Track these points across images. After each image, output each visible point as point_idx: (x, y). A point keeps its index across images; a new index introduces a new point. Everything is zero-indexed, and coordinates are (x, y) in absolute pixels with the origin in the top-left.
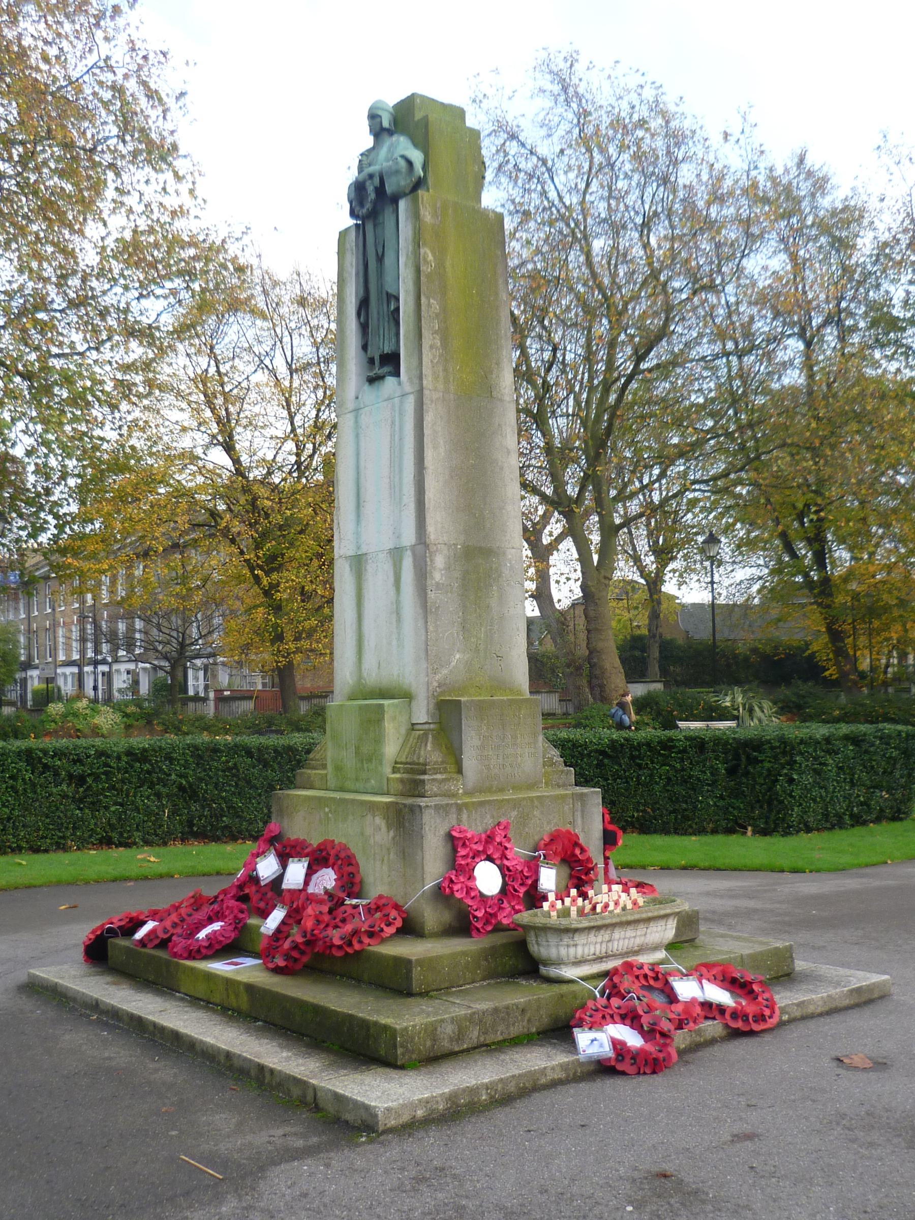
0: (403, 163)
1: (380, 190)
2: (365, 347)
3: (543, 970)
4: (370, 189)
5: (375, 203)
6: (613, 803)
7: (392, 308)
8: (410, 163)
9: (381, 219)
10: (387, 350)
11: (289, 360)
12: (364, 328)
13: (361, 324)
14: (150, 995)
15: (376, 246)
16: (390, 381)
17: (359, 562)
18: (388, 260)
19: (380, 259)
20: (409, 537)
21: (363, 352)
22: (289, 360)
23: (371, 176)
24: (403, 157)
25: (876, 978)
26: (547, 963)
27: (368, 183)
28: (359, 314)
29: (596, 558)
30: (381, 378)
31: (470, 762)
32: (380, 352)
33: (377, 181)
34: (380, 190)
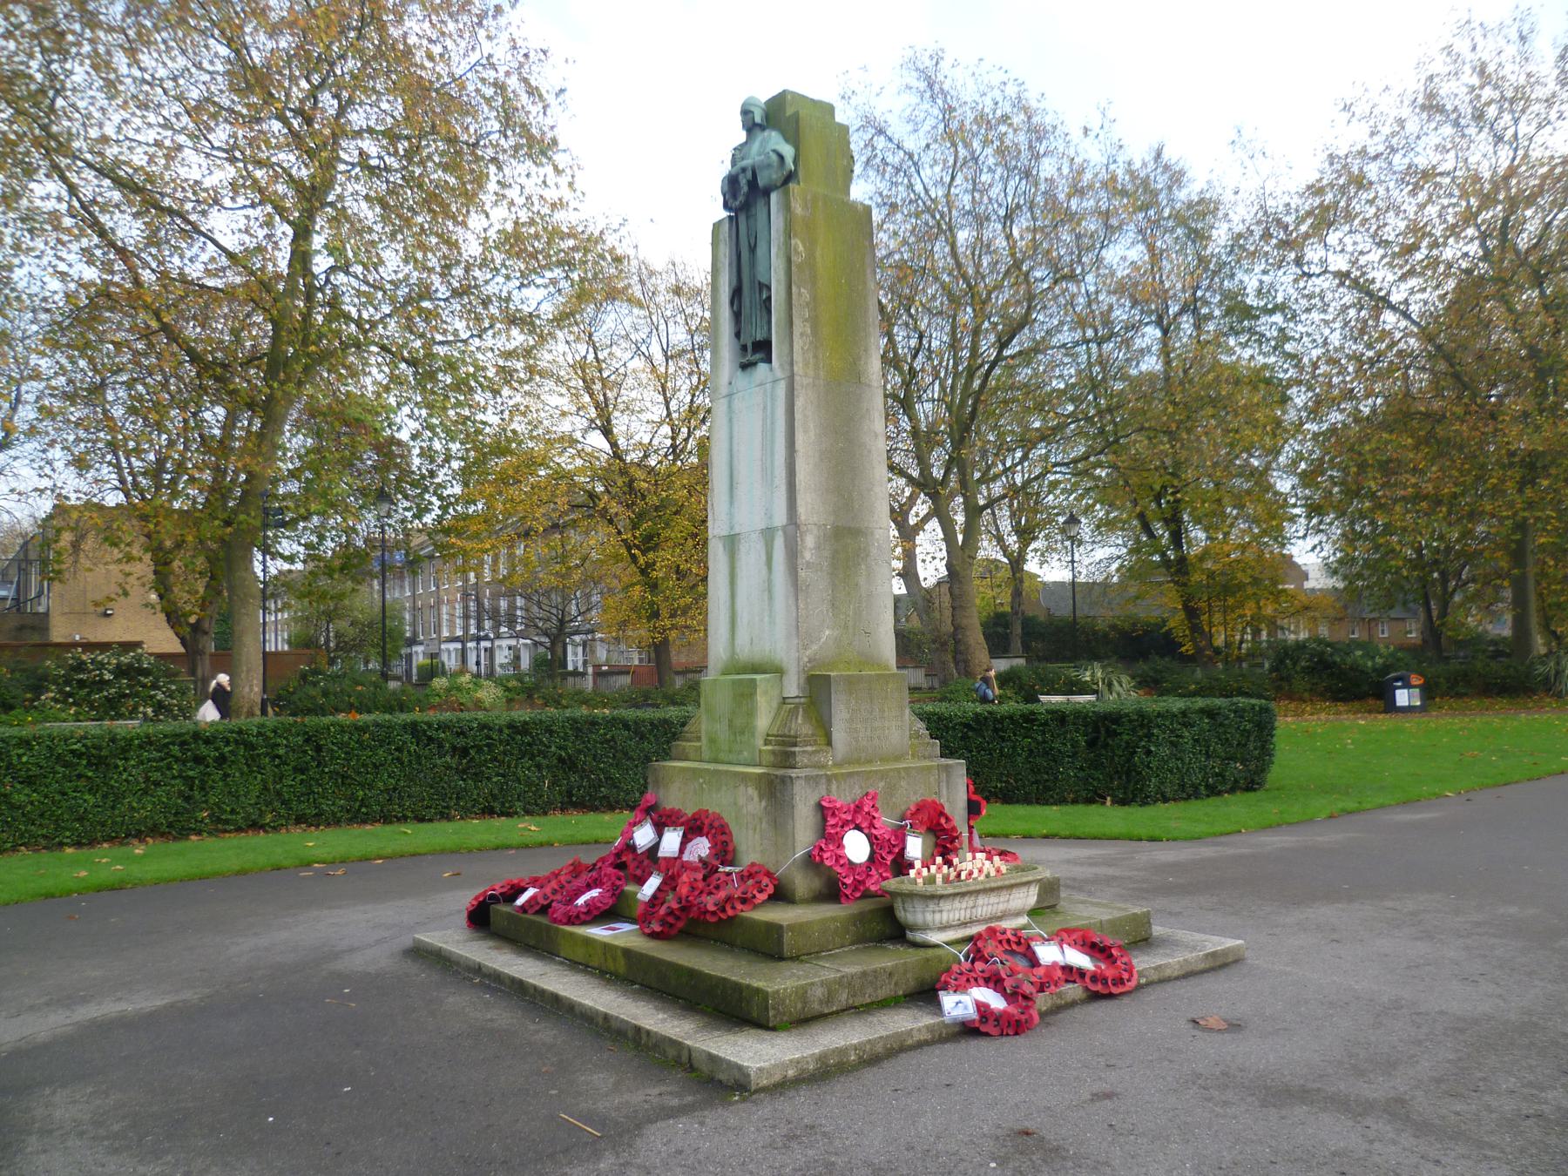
0: (774, 157)
1: (753, 183)
2: (738, 335)
4: (743, 182)
5: (748, 196)
8: (781, 157)
12: (737, 316)
16: (762, 367)
17: (732, 542)
18: (761, 251)
19: (753, 249)
20: (780, 518)
23: (744, 170)
24: (774, 151)
28: (732, 303)
31: (839, 734)
33: (749, 175)
34: (753, 183)
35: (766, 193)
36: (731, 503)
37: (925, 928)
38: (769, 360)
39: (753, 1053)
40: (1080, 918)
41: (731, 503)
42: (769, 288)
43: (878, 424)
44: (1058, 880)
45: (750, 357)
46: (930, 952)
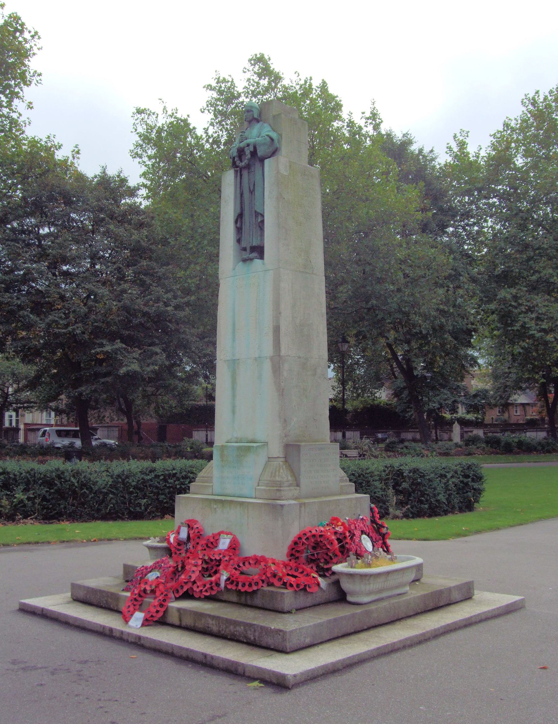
0: (268, 139)
1: (254, 153)
2: (239, 241)
3: (349, 598)
4: (248, 152)
5: (249, 160)
6: (81, 516)
7: (259, 220)
8: (272, 139)
9: (252, 169)
10: (255, 244)
11: (252, 189)
12: (239, 230)
13: (237, 227)
14: (221, 677)
15: (249, 184)
16: (257, 262)
17: (234, 363)
18: (257, 193)
19: (252, 192)
20: (268, 350)
21: (237, 244)
22: (252, 189)
23: (248, 145)
24: (268, 136)
25: (517, 598)
26: (353, 594)
27: (246, 149)
28: (236, 222)
29: (405, 366)
30: (251, 259)
31: (304, 481)
32: (250, 245)
33: (252, 149)
34: (254, 153)
35: (262, 160)
36: (234, 340)
37: (353, 594)
38: (261, 257)
39: (289, 666)
40: (367, 545)
41: (234, 340)
42: (263, 216)
43: (456, 462)
44: (213, 429)
45: (246, 255)
46: (247, 576)
